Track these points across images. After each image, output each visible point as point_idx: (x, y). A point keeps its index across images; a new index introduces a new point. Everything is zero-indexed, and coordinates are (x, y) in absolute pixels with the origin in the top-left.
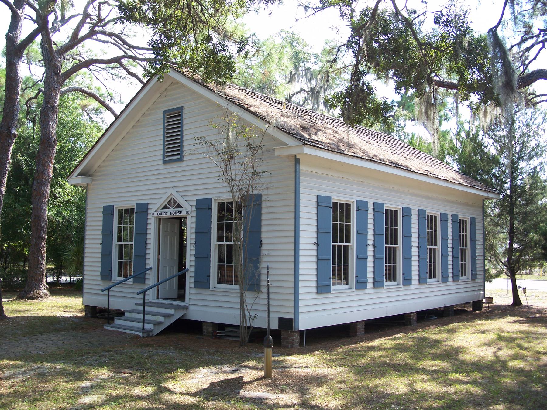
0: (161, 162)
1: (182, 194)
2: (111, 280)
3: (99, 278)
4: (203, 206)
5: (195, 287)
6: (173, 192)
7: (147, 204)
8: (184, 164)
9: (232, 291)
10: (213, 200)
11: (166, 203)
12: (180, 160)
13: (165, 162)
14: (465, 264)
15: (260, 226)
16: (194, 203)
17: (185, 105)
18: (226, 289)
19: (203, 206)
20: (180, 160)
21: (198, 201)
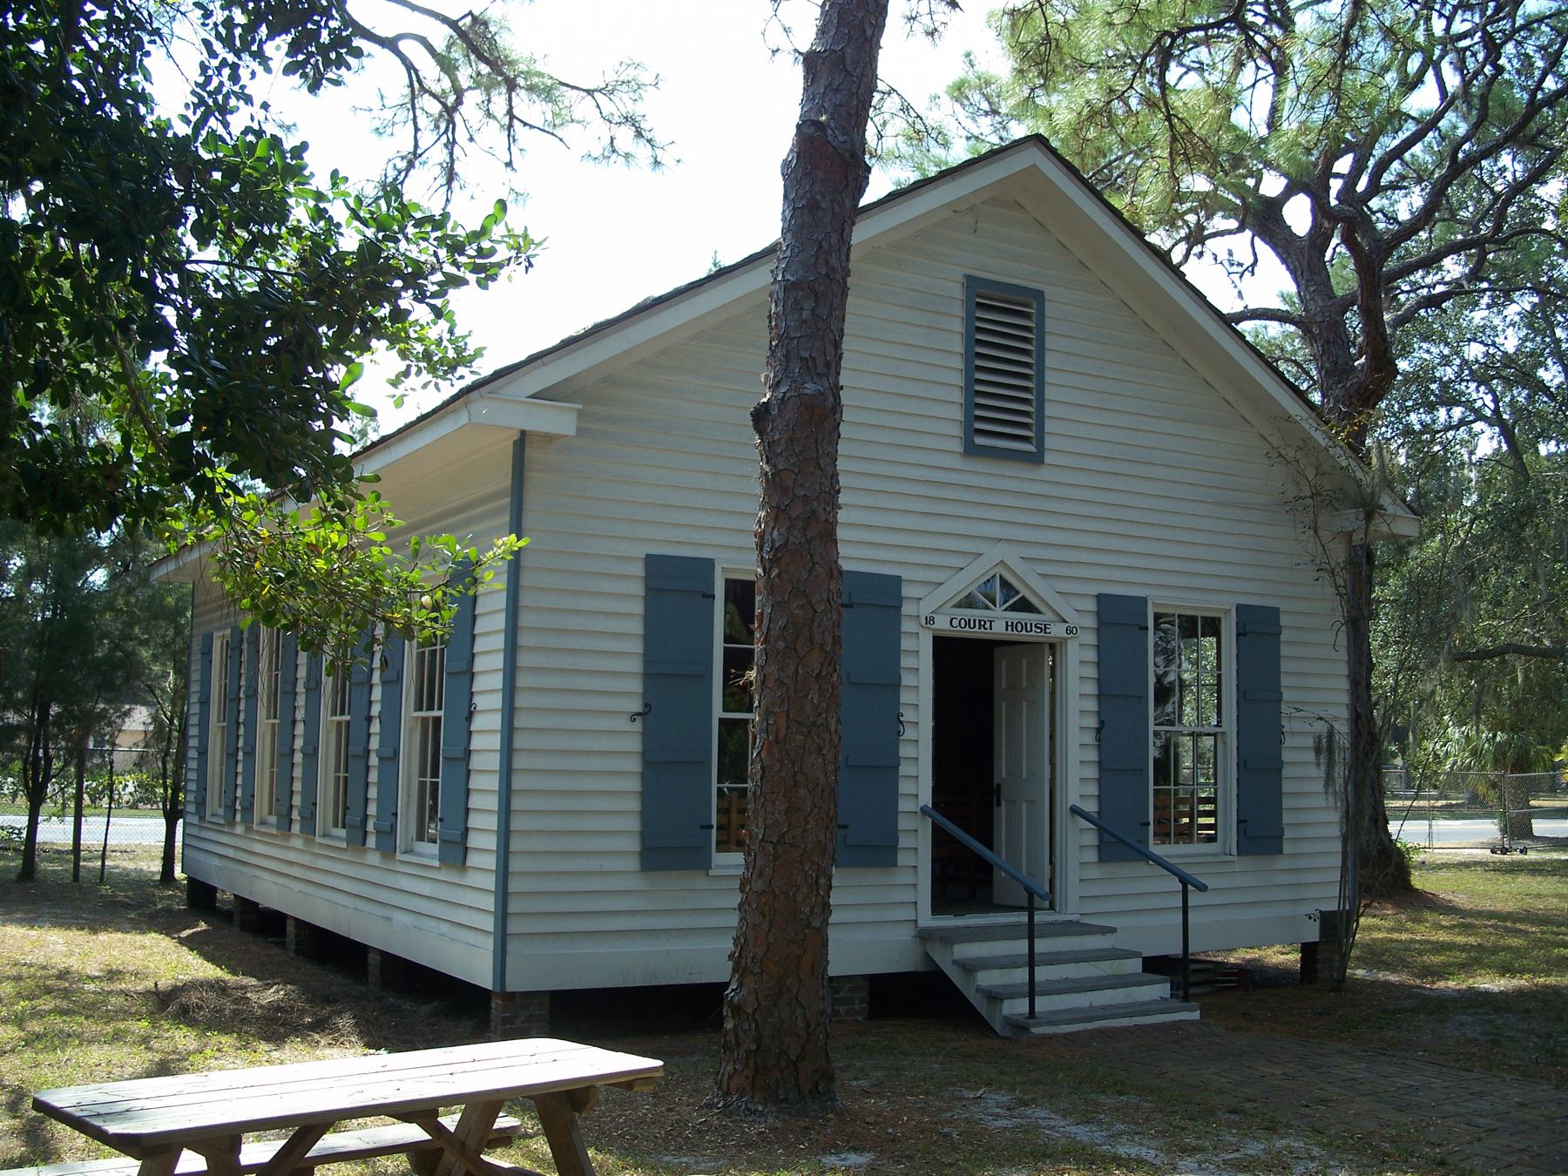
3: (633, 864)
4: (1118, 618)
5: (1102, 859)
6: (1012, 556)
7: (896, 581)
8: (1043, 473)
11: (1024, 592)
13: (971, 450)
14: (423, 774)
20: (1036, 459)
21: (651, 562)
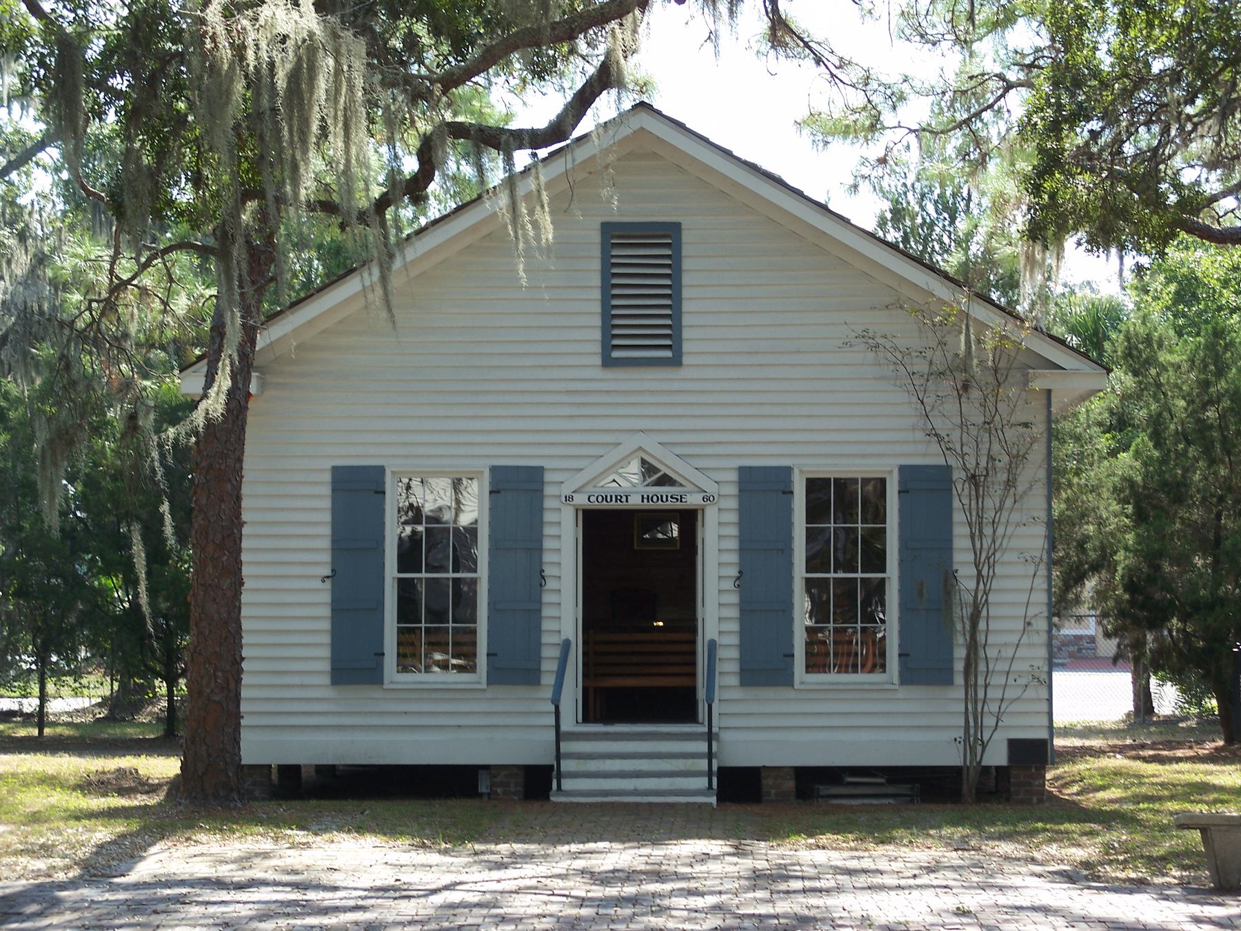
0: (598, 360)
1: (679, 451)
2: (382, 683)
3: (327, 680)
8: (683, 373)
9: (867, 687)
10: (796, 471)
12: (676, 362)
15: (539, 538)
16: (733, 476)
17: (686, 221)
18: (838, 683)
19: (761, 487)
20: (676, 362)
21: (335, 470)
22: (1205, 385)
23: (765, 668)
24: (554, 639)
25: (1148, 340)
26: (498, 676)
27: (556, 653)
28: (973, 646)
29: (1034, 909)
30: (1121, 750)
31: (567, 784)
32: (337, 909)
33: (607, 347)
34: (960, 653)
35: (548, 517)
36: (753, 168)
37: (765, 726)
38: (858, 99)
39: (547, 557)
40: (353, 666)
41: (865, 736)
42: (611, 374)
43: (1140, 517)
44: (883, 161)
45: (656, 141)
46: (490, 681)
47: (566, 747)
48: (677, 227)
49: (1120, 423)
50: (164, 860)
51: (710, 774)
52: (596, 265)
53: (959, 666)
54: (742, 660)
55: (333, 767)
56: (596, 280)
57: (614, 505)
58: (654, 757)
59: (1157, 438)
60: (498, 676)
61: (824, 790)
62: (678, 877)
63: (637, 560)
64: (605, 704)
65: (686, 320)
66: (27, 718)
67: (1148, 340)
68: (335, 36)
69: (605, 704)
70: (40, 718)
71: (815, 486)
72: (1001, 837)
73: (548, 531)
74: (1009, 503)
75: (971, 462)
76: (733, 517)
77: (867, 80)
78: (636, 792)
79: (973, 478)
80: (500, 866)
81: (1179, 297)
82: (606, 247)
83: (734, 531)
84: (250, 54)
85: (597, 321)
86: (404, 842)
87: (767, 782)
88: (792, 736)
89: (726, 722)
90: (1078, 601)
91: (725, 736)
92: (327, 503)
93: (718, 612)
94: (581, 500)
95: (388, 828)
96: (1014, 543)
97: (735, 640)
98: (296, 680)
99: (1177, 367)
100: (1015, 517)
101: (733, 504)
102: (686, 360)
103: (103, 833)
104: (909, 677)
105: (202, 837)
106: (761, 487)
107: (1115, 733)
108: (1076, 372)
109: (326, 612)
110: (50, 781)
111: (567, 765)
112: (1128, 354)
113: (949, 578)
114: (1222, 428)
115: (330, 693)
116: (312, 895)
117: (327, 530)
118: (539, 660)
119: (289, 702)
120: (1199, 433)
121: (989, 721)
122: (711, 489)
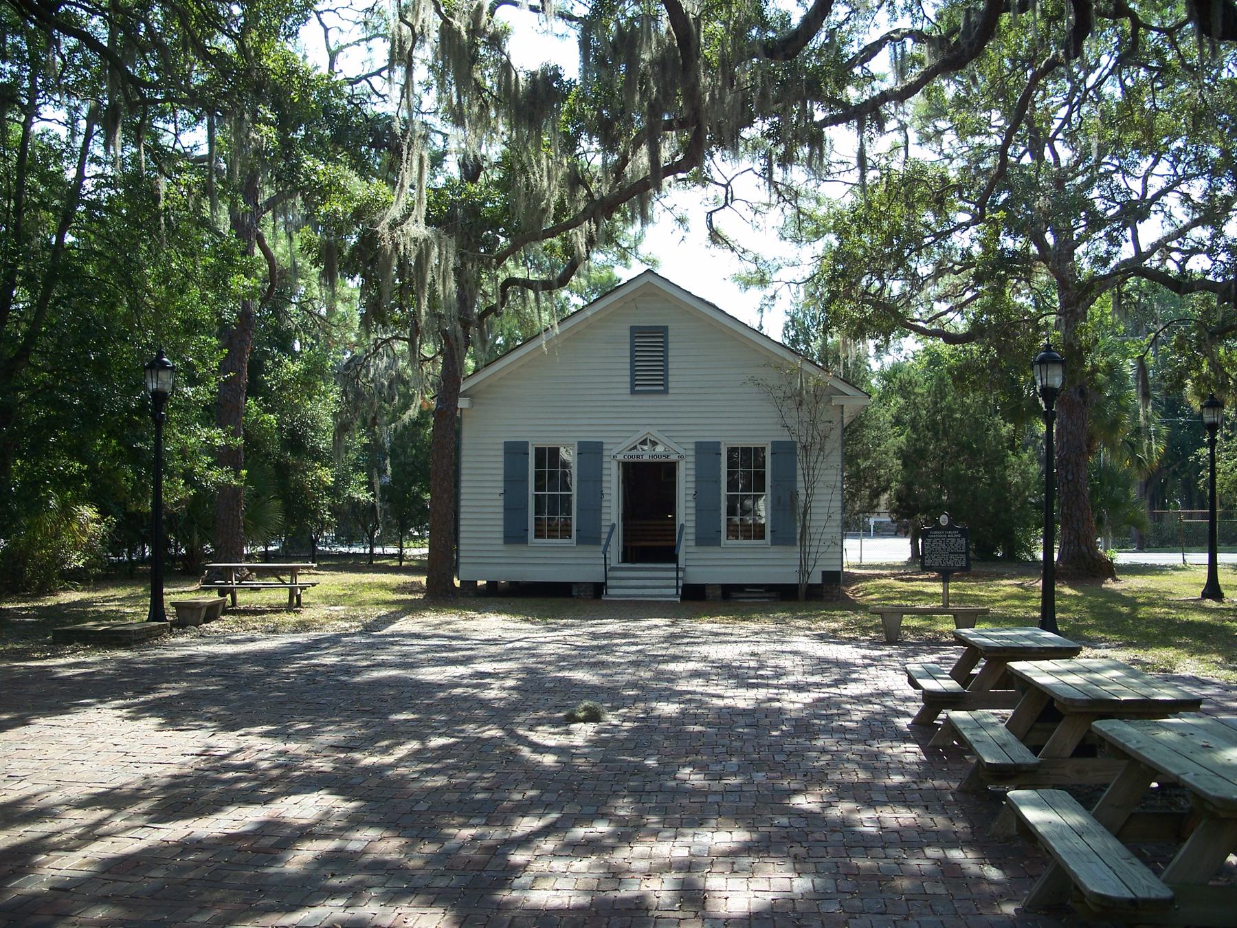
3: (501, 542)
8: (670, 397)
12: (666, 392)
16: (693, 446)
19: (706, 451)
20: (666, 392)
22: (935, 403)
23: (707, 538)
24: (608, 523)
25: (910, 382)
26: (582, 540)
27: (608, 530)
28: (804, 527)
29: (791, 652)
30: (893, 575)
31: (610, 592)
32: (460, 649)
33: (633, 385)
34: (799, 530)
35: (605, 466)
36: (702, 300)
37: (701, 564)
38: (753, 268)
39: (604, 485)
40: (514, 535)
41: (754, 569)
42: (636, 398)
43: (905, 465)
44: (773, 297)
45: (652, 285)
46: (773, 543)
47: (610, 574)
48: (665, 329)
49: (898, 421)
50: (406, 624)
51: (677, 587)
52: (628, 346)
53: (798, 536)
54: (696, 533)
55: (517, 583)
56: (628, 353)
57: (636, 460)
58: (655, 579)
59: (914, 428)
60: (582, 540)
61: (735, 595)
62: (635, 636)
63: (649, 485)
64: (634, 553)
65: (670, 372)
66: (391, 556)
67: (910, 382)
68: (439, 237)
69: (634, 553)
70: (401, 557)
71: (732, 451)
72: (802, 618)
73: (605, 472)
74: (820, 459)
75: (803, 440)
76: (692, 466)
77: (756, 259)
78: (643, 596)
79: (805, 447)
80: (554, 630)
81: (930, 363)
82: (633, 337)
83: (693, 472)
84: (402, 247)
85: (628, 373)
86: (519, 618)
87: (708, 591)
88: (718, 569)
89: (689, 563)
90: (878, 505)
91: (689, 570)
92: (502, 459)
93: (685, 512)
94: (620, 457)
95: (513, 612)
96: (823, 478)
97: (693, 524)
98: (488, 542)
99: (923, 395)
100: (824, 466)
101: (693, 459)
102: (670, 391)
103: (384, 611)
104: (775, 542)
105: (428, 614)
106: (706, 451)
107: (899, 567)
108: (854, 397)
109: (502, 510)
110: (383, 586)
111: (609, 583)
112: (901, 388)
113: (794, 495)
114: (944, 424)
115: (503, 548)
116: (454, 643)
117: (502, 472)
118: (600, 533)
119: (484, 549)
120: (933, 426)
121: (811, 563)
122: (682, 452)
